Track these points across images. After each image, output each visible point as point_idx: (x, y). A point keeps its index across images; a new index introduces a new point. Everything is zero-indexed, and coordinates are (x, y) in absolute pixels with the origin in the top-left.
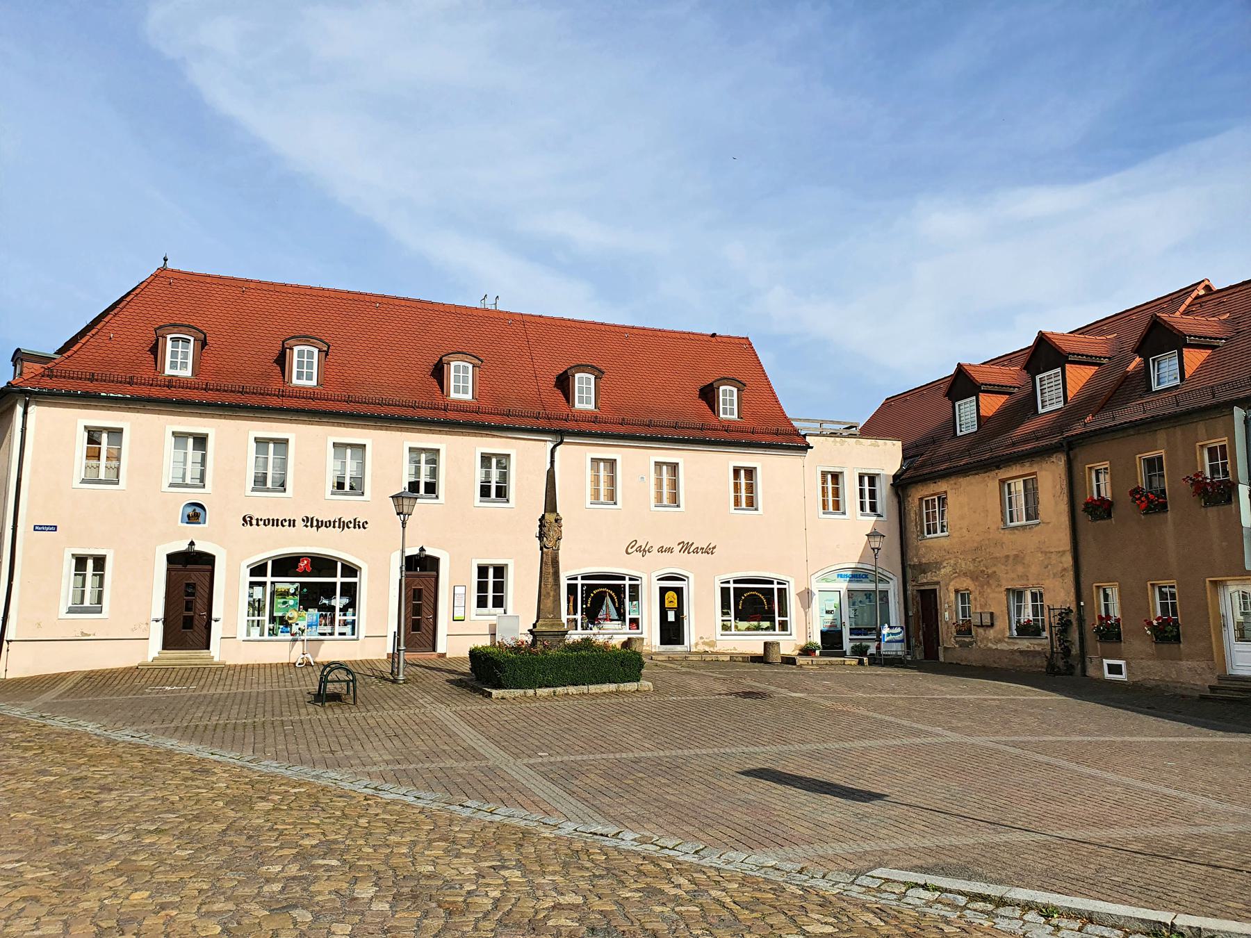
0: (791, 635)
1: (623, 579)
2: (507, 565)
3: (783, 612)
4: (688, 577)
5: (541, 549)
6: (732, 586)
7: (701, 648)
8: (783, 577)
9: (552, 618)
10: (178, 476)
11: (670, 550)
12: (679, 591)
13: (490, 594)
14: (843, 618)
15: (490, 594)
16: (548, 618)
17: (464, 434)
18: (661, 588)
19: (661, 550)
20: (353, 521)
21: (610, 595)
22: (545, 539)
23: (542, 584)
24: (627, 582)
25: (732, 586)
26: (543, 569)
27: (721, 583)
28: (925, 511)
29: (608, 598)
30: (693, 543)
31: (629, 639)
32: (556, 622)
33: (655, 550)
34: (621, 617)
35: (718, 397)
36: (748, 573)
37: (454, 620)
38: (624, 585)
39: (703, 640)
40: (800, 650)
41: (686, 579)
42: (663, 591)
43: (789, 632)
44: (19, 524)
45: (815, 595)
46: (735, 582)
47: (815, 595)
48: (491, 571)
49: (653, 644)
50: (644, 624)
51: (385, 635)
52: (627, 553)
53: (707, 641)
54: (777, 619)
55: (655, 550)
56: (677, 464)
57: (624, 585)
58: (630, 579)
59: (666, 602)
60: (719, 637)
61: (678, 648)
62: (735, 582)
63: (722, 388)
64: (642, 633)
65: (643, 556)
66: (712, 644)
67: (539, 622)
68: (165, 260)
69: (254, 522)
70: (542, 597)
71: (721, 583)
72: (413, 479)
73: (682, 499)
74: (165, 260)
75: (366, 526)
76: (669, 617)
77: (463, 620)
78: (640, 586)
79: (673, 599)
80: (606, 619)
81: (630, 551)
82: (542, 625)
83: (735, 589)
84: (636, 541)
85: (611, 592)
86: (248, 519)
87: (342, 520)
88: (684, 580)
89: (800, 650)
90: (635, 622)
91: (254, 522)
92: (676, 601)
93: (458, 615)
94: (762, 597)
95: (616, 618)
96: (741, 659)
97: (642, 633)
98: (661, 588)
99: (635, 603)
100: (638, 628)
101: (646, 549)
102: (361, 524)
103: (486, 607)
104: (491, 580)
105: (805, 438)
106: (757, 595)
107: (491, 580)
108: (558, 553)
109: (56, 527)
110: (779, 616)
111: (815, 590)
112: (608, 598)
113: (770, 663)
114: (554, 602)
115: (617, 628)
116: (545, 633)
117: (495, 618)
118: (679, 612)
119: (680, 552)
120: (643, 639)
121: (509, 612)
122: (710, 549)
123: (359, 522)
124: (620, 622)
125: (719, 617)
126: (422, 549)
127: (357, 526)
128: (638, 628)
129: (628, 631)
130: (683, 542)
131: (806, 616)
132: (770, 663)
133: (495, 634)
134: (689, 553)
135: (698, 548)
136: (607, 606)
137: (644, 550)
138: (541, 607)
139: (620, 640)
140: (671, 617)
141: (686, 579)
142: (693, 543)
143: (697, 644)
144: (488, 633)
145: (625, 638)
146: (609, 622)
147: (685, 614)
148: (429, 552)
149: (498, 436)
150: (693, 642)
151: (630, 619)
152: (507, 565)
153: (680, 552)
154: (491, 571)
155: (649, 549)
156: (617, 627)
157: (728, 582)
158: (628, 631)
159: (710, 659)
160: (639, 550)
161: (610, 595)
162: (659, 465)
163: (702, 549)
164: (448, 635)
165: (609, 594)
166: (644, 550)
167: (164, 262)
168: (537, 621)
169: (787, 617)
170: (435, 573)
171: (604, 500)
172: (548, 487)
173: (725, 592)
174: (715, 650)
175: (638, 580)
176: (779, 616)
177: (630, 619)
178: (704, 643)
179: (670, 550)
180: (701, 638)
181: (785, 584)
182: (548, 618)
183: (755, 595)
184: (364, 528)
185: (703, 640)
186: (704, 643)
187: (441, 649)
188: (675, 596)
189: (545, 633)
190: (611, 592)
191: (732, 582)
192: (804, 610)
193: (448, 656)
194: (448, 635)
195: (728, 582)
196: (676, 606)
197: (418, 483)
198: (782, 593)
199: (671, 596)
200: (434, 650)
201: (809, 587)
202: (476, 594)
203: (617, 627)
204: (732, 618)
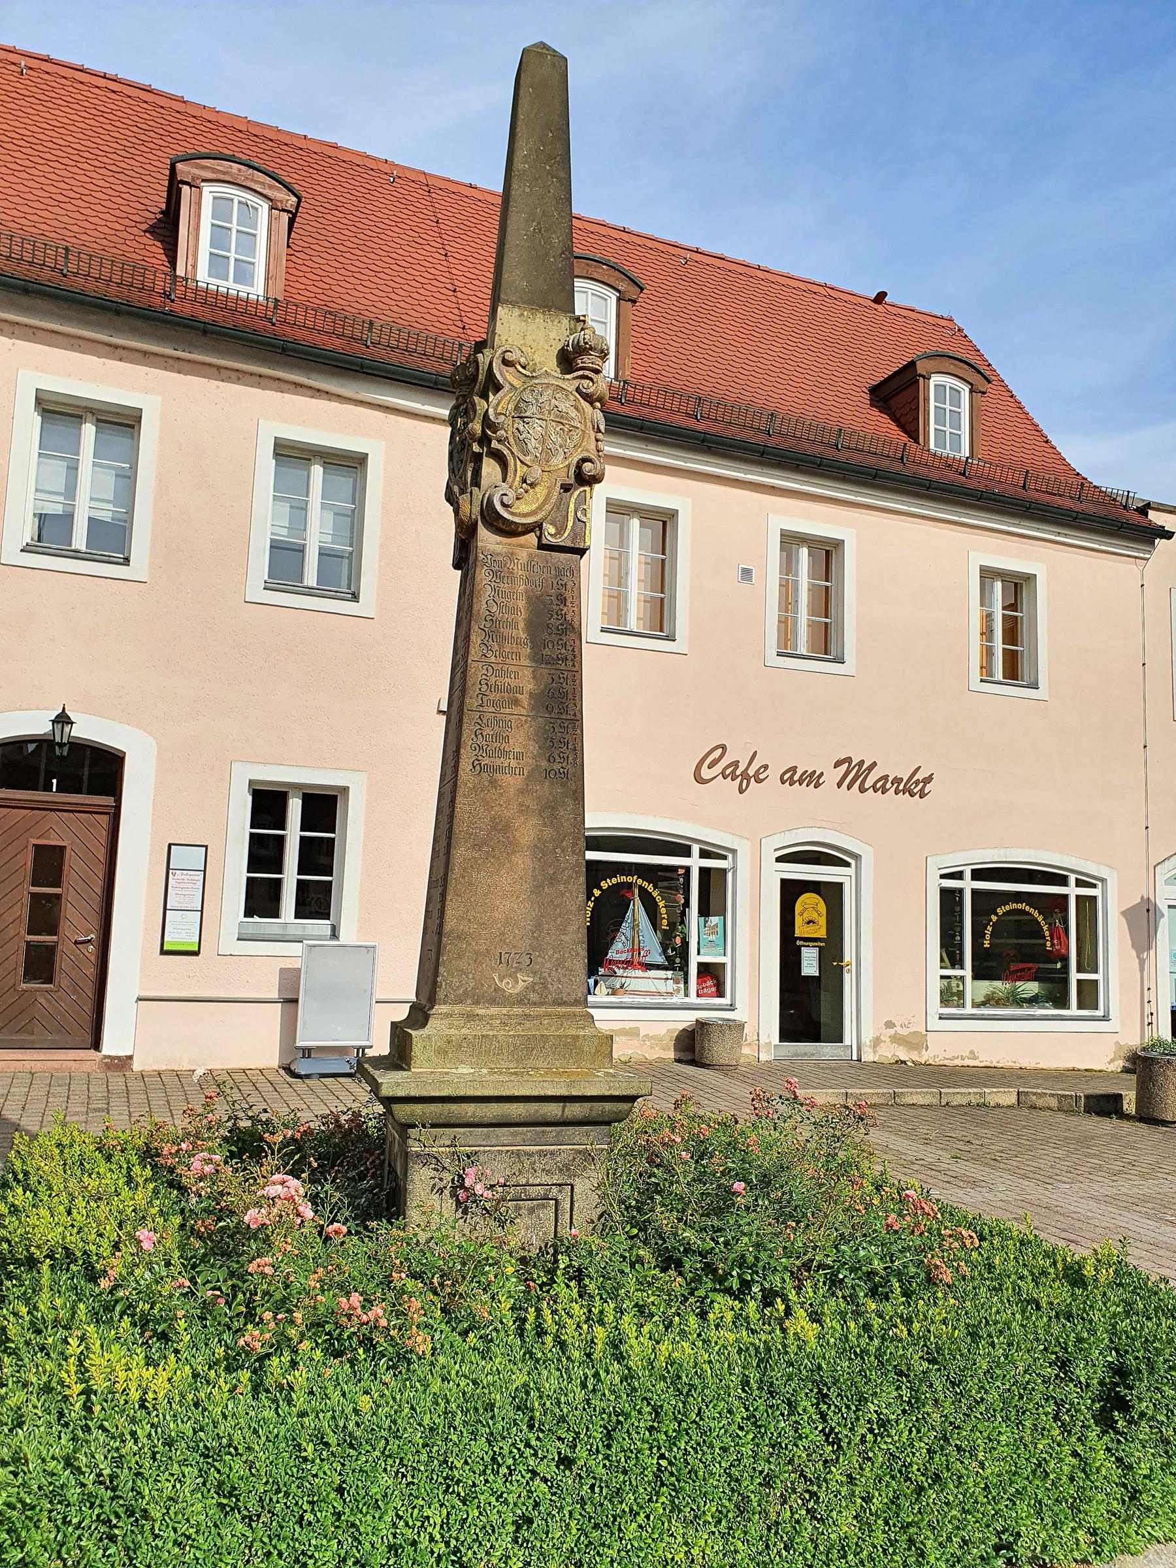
0: (1105, 1018)
1: (686, 851)
2: (345, 790)
3: (1088, 962)
4: (857, 857)
5: (464, 555)
6: (968, 885)
7: (889, 1052)
8: (1091, 868)
9: (521, 1000)
11: (813, 779)
12: (832, 894)
13: (290, 876)
15: (290, 876)
16: (497, 998)
17: (225, 373)
18: (785, 883)
19: (790, 777)
21: (644, 893)
22: (490, 468)
23: (465, 764)
24: (695, 863)
25: (968, 885)
26: (476, 671)
27: (943, 877)
29: (637, 909)
30: (874, 764)
31: (701, 1025)
32: (550, 1029)
33: (774, 773)
34: (676, 960)
35: (926, 400)
36: (1008, 851)
38: (688, 869)
39: (892, 1032)
40: (1128, 1059)
41: (852, 862)
42: (791, 891)
43: (1100, 1013)
45: (1163, 916)
46: (978, 875)
47: (1163, 916)
48: (295, 807)
49: (763, 1040)
50: (739, 982)
52: (699, 780)
53: (904, 1032)
54: (1074, 976)
55: (774, 773)
56: (838, 544)
57: (688, 869)
58: (704, 854)
59: (798, 921)
60: (934, 1023)
61: (825, 1050)
62: (978, 875)
63: (935, 379)
64: (732, 1007)
65: (741, 791)
66: (916, 1042)
67: (435, 1026)
70: (461, 853)
71: (943, 877)
72: (55, 508)
73: (851, 640)
76: (804, 963)
77: (196, 954)
78: (730, 875)
79: (815, 916)
80: (628, 964)
81: (706, 773)
82: (448, 1049)
83: (975, 893)
84: (724, 747)
85: (650, 888)
88: (848, 865)
89: (1128, 1059)
90: (712, 974)
92: (823, 921)
93: (181, 933)
94: (1040, 919)
95: (660, 960)
96: (1053, 1103)
97: (732, 1007)
98: (785, 883)
99: (714, 920)
100: (720, 993)
101: (751, 772)
103: (276, 915)
104: (293, 833)
105: (1146, 515)
106: (1028, 913)
107: (293, 833)
108: (575, 572)
110: (1079, 970)
111: (1163, 906)
112: (637, 909)
113: (1164, 1123)
114: (537, 888)
115: (663, 989)
116: (470, 1111)
117: (296, 949)
118: (832, 948)
119: (839, 785)
120: (741, 1026)
121: (347, 935)
122: (917, 783)
124: (669, 974)
125: (935, 970)
126: (63, 719)
128: (720, 993)
129: (693, 999)
130: (849, 760)
131: (1142, 970)
132: (1164, 1123)
133: (296, 1001)
134: (862, 790)
135: (886, 777)
136: (635, 926)
137: (745, 775)
138: (450, 923)
139: (672, 1026)
140: (810, 965)
141: (852, 862)
142: (874, 764)
143: (877, 1042)
144: (275, 995)
145: (690, 1018)
146: (639, 973)
147: (847, 958)
148: (85, 729)
149: (329, 395)
150: (867, 1037)
151: (700, 965)
152: (345, 790)
153: (839, 785)
154: (295, 807)
155: (757, 772)
156: (662, 986)
157: (958, 876)
158: (693, 999)
159: (964, 1102)
160: (732, 772)
161: (644, 893)
162: (790, 540)
163: (897, 780)
164: (140, 999)
165: (642, 890)
166: (745, 775)
168: (420, 1014)
169: (1096, 972)
170: (110, 801)
171: (638, 628)
172: (521, 152)
173: (950, 900)
174: (924, 1057)
175: (725, 858)
176: (1079, 970)
177: (700, 965)
178: (897, 1040)
179: (813, 779)
180: (890, 1025)
181: (1094, 886)
182: (497, 998)
183: (1023, 912)
185: (892, 1032)
186: (897, 1040)
187: (112, 1044)
188: (822, 907)
189: (470, 1111)
190: (650, 888)
191: (968, 875)
192: (1138, 957)
193: (137, 1066)
194: (140, 999)
195: (958, 876)
196: (822, 933)
197: (68, 518)
198: (1087, 905)
199: (809, 906)
200: (96, 1045)
201: (1152, 898)
202: (245, 875)
203: (662, 986)
204: (967, 972)
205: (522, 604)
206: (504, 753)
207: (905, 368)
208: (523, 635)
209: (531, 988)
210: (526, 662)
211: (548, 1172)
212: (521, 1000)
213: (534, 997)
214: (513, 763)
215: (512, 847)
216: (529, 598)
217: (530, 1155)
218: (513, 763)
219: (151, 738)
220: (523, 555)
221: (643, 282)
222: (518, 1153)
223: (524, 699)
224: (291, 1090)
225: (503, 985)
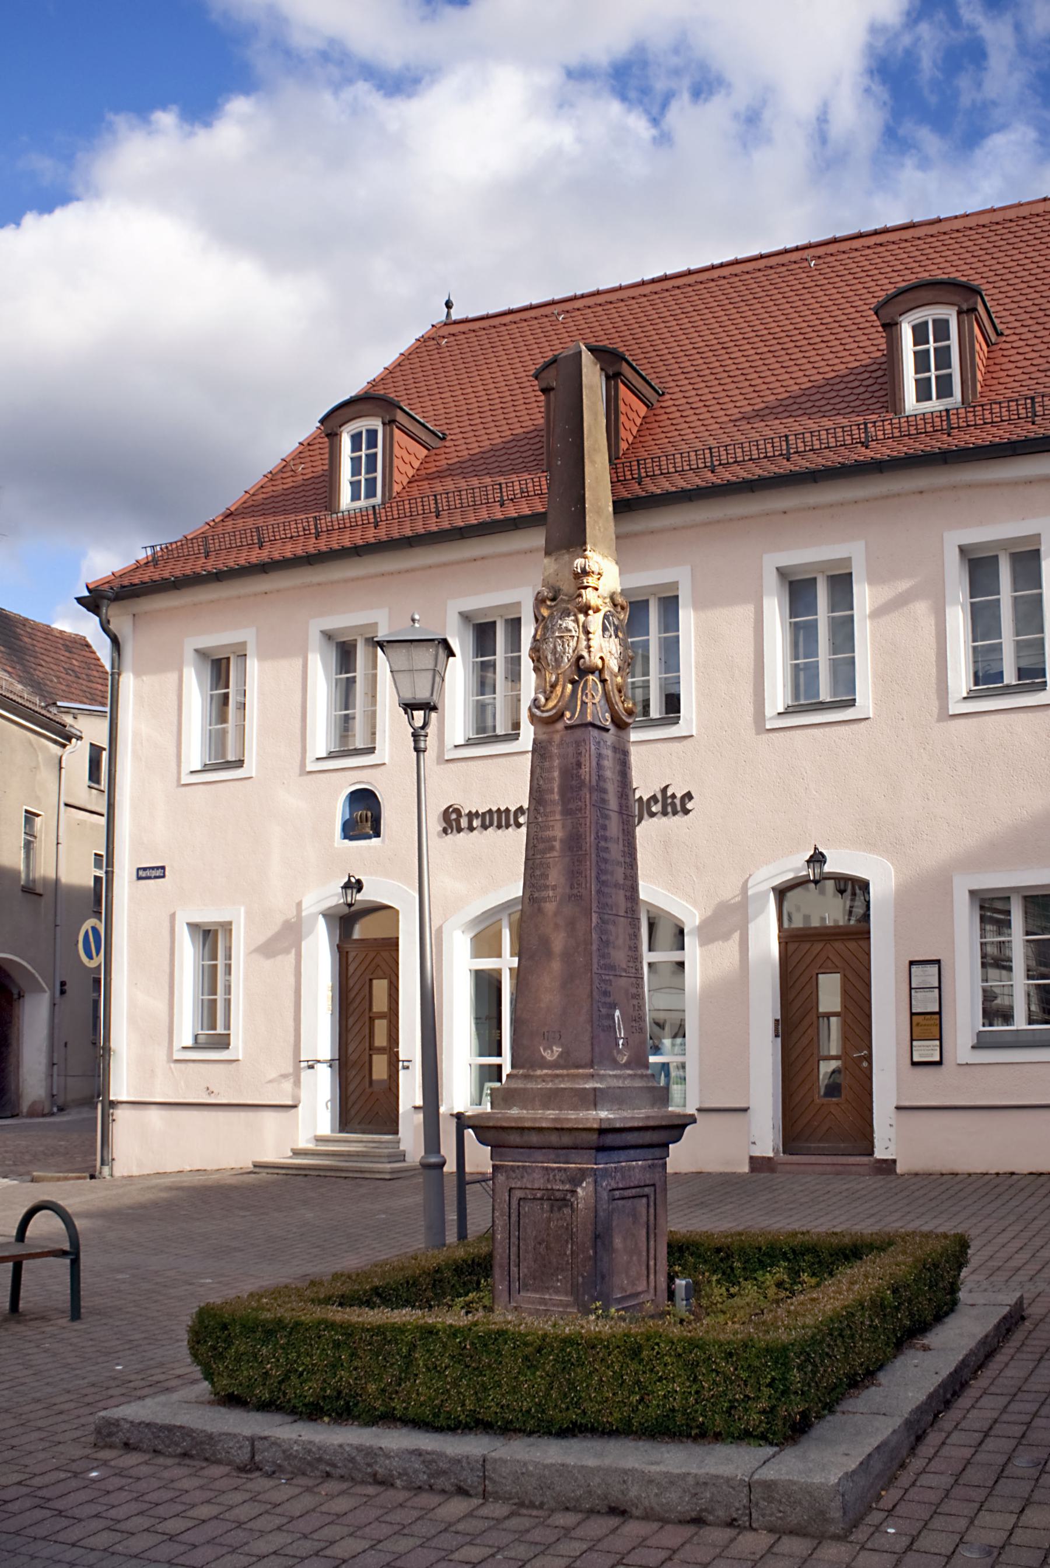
9: (554, 1065)
10: (643, 748)
14: (58, 918)
20: (659, 797)
28: (954, 342)
37: (914, 1064)
44: (417, 881)
51: (743, 1105)
68: (449, 305)
69: (464, 822)
74: (449, 305)
75: (689, 806)
86: (454, 816)
87: (669, 793)
91: (464, 822)
102: (677, 801)
109: (163, 868)
123: (673, 796)
127: (669, 809)
167: (446, 310)
184: (686, 812)
193: (900, 1169)
205: (556, 774)
206: (546, 887)
207: (643, 601)
208: (557, 798)
209: (561, 1056)
210: (558, 817)
211: (563, 1182)
212: (554, 1065)
213: (562, 1062)
214: (551, 893)
215: (549, 954)
216: (560, 769)
217: (553, 1169)
218: (551, 893)
219: (854, 1466)
220: (557, 738)
221: (976, 283)
222: (547, 1168)
223: (557, 845)
224: (633, 1529)
225: (545, 1054)
